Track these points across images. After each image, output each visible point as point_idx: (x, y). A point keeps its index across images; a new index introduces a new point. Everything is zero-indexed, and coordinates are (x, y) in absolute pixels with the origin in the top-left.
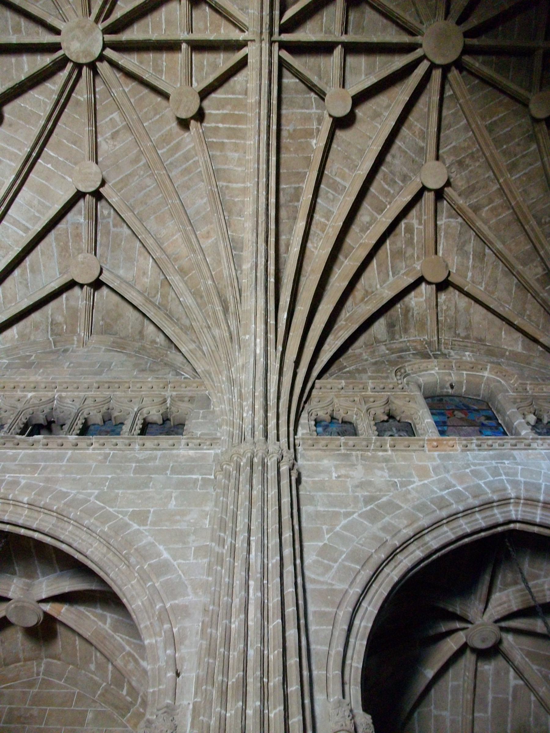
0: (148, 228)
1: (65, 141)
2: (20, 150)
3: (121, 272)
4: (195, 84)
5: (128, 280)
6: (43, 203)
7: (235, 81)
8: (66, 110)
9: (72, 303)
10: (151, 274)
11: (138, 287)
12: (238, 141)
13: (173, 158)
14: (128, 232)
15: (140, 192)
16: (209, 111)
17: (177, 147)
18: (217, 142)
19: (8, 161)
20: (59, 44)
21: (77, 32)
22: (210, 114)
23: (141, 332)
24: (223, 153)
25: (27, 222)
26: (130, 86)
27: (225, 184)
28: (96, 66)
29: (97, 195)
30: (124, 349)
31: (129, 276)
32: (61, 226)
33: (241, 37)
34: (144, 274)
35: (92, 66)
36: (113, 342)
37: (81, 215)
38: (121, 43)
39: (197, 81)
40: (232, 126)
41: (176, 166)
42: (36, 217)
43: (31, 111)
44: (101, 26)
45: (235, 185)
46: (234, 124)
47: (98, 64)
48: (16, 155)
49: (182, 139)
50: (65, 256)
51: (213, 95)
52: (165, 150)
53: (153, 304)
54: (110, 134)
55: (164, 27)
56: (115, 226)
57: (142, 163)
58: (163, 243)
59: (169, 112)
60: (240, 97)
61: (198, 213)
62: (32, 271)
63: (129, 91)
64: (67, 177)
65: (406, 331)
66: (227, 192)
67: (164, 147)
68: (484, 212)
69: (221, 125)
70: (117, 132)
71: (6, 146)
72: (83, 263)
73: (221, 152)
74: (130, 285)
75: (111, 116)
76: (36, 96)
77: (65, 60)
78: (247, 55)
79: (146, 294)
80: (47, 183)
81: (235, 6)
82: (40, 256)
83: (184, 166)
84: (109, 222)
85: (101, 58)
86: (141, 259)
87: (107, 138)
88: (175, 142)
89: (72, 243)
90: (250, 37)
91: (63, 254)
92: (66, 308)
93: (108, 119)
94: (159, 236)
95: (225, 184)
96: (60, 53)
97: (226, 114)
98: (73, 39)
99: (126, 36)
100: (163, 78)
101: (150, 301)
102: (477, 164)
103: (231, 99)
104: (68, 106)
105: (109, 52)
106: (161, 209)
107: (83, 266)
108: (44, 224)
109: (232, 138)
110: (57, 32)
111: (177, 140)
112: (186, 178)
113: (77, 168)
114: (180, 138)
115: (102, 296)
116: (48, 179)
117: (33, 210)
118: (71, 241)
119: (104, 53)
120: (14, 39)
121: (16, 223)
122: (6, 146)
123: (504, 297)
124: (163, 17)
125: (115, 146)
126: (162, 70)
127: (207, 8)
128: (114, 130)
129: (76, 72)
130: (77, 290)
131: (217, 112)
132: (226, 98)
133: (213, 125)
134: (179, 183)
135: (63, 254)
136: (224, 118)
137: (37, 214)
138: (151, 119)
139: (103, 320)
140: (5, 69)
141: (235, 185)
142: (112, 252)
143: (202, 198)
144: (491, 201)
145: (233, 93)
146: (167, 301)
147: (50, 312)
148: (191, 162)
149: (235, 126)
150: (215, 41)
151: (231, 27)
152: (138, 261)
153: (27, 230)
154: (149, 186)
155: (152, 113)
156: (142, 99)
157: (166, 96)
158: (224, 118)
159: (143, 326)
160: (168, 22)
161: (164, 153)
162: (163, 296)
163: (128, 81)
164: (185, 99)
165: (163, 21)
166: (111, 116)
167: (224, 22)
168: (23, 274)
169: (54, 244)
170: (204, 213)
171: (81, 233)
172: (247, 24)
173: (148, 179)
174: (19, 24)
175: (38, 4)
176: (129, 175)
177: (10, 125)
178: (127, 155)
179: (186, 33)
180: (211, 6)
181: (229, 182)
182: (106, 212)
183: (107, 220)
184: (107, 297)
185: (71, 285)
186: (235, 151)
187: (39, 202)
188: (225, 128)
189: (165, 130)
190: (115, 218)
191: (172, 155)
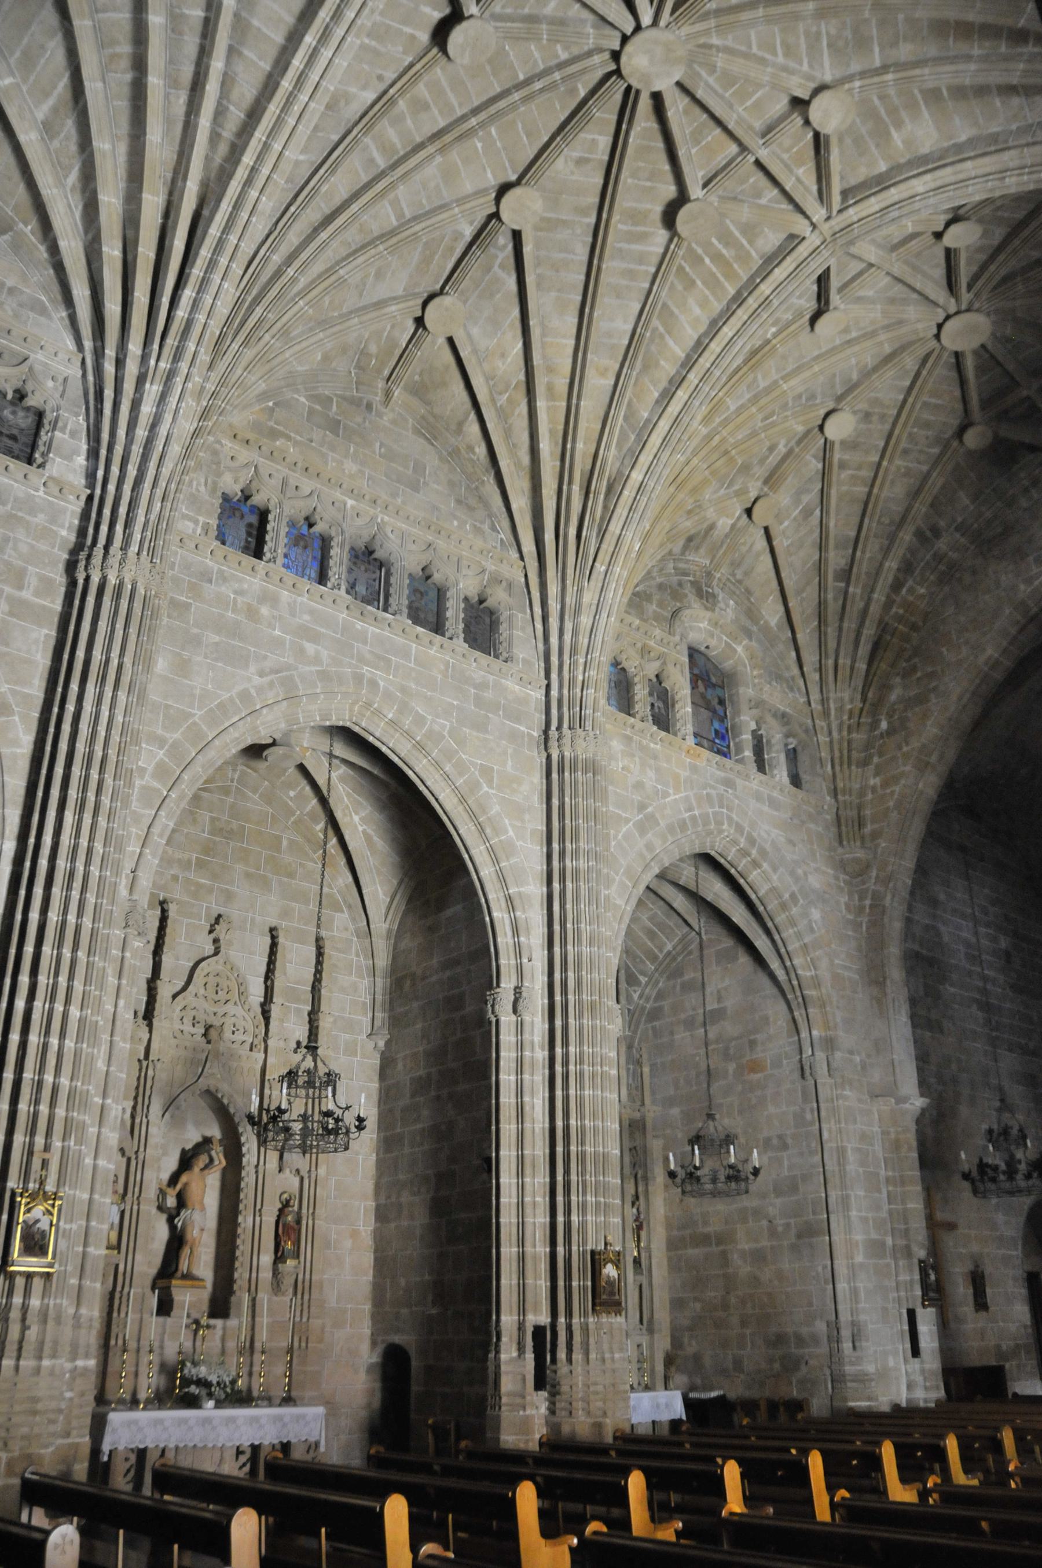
3: (475, 331)
12: (711, 298)
17: (642, 237)
18: (687, 274)
19: (436, 112)
23: (460, 424)
30: (435, 438)
34: (503, 355)
36: (423, 417)
40: (719, 275)
45: (671, 343)
56: (502, 266)
60: (754, 254)
65: (697, 548)
66: (657, 341)
68: (845, 475)
69: (707, 261)
70: (587, 160)
71: (448, 90)
73: (685, 289)
75: (596, 137)
83: (632, 266)
95: (661, 329)
102: (879, 427)
103: (742, 246)
122: (448, 90)
123: (798, 565)
125: (572, 173)
137: (424, 201)
139: (421, 375)
141: (671, 343)
143: (625, 322)
144: (859, 468)
145: (750, 242)
149: (722, 279)
152: (503, 334)
159: (467, 418)
162: (510, 400)
165: (754, 98)
167: (811, 165)
169: (419, 249)
181: (669, 333)
186: (701, 306)
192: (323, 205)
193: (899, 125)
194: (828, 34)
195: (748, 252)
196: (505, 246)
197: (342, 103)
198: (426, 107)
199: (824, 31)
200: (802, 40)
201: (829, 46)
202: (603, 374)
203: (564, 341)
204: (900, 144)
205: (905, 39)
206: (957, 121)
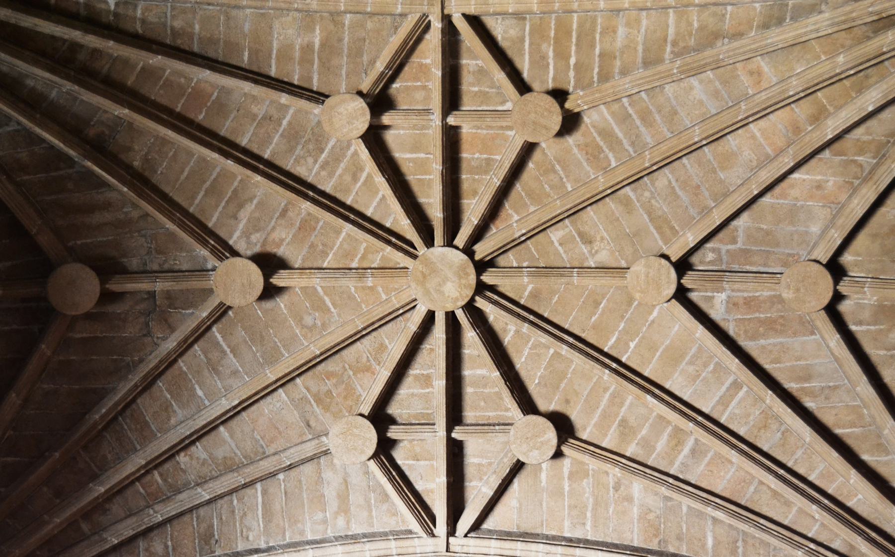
0: (739, 182)
1: (593, 319)
2: (606, 390)
3: (815, 229)
4: (508, 106)
5: (829, 217)
6: (692, 357)
7: (503, 38)
8: (546, 315)
9: (866, 315)
10: (820, 174)
11: (843, 197)
12: (599, 29)
13: (625, 141)
14: (745, 217)
15: (678, 197)
16: (550, 81)
18: (600, 66)
19: (623, 409)
20: (447, 313)
21: (431, 284)
22: (554, 79)
24: (618, 54)
25: (723, 384)
26: (510, 211)
27: (669, 49)
28: (481, 260)
29: (683, 266)
31: (823, 214)
32: (731, 330)
33: (437, 26)
34: (819, 187)
35: (481, 266)
37: (713, 297)
38: (446, 220)
39: (503, 103)
40: (574, 40)
41: (637, 136)
42: (715, 370)
43: (545, 369)
44: (422, 250)
45: (671, 31)
46: (571, 36)
47: (478, 257)
48: (613, 396)
49: (594, 127)
50: (782, 325)
51: (525, 75)
52: (611, 155)
53: (874, 169)
54: (583, 247)
55: (422, 155)
56: (734, 241)
57: (631, 194)
58: (767, 156)
59: (549, 148)
61: (716, 94)
62: (808, 378)
63: (517, 213)
64: (651, 318)
66: (682, 44)
67: (607, 157)
69: (573, 61)
70: (581, 235)
72: (798, 290)
73: (615, 58)
74: (838, 212)
75: (556, 244)
76: (523, 360)
77: (470, 308)
78: (464, 15)
79: (856, 182)
80: (661, 350)
81: (391, 39)
82: (782, 365)
83: (638, 122)
84: (728, 251)
85: (468, 251)
86: (794, 193)
87: (590, 252)
88: (598, 139)
89: (760, 312)
90: (437, 9)
91: (779, 327)
92: (874, 325)
93: (560, 248)
94: (755, 163)
95: (669, 49)
96: (461, 315)
97: (554, 51)
98: (442, 293)
99: (436, 213)
100: (498, 157)
101: (870, 173)
103: (531, 44)
104: (540, 312)
105: (461, 240)
106: (709, 161)
107: (802, 290)
108: (729, 353)
109: (594, 38)
110: (430, 317)
111: (595, 134)
112: (657, 117)
113: (637, 296)
114: (592, 130)
115: (856, 264)
116: (653, 349)
117: (704, 374)
118: (757, 315)
119: (461, 247)
120: (440, 384)
121: (724, 402)
124: (408, 156)
125: (602, 239)
126: (486, 159)
127: (394, 86)
128: (578, 239)
129: (489, 294)
130: (844, 307)
131: (551, 67)
132: (530, 53)
133: (572, 74)
134: (665, 130)
135: (779, 327)
136: (562, 55)
137: (711, 367)
138: (561, 179)
140: (482, 404)
141: (671, 31)
142: (777, 245)
143: (691, 88)
145: (522, 40)
146: (870, 142)
147: (882, 352)
148: (631, 111)
150: (443, 69)
151: (422, 46)
153: (736, 386)
154: (670, 182)
155: (552, 176)
156: (530, 194)
157: (529, 149)
158: (562, 55)
160: (415, 148)
161: (615, 157)
162: (861, 151)
163: (503, 214)
164: (532, 116)
165: (414, 156)
166: (556, 244)
167: (415, 59)
168: (812, 394)
169: (762, 342)
170: (717, 83)
171: (745, 298)
172: (418, 15)
173: (657, 184)
174: (416, 377)
175: (390, 347)
176: (649, 214)
177: (567, 401)
178: (618, 219)
179: (432, 117)
180: (393, 79)
181: (665, 40)
182: (710, 256)
183: (723, 252)
184: (858, 255)
185: (832, 311)
186: (615, 32)
187: (691, 363)
188: (577, 52)
189: (579, 156)
190: (721, 241)
191: (620, 143)
192: (752, 489)
193: (308, 48)
194: (316, 161)
195: (531, 34)
196: (713, 250)
197: (651, 516)
198: (624, 423)
199: (317, 166)
200: (339, 171)
201: (322, 151)
202: (757, 74)
203: (758, 134)
204: (318, 31)
205: (255, 116)
206: (247, 27)
